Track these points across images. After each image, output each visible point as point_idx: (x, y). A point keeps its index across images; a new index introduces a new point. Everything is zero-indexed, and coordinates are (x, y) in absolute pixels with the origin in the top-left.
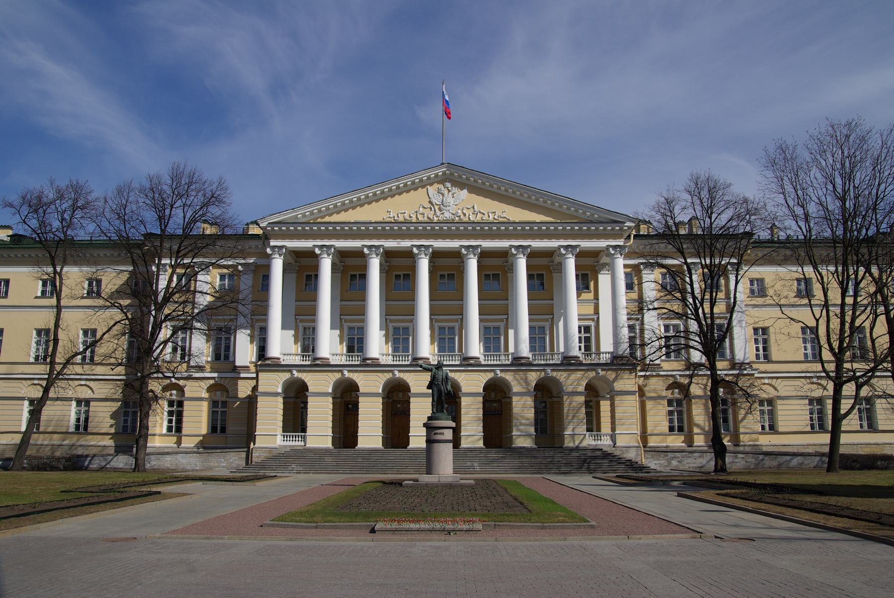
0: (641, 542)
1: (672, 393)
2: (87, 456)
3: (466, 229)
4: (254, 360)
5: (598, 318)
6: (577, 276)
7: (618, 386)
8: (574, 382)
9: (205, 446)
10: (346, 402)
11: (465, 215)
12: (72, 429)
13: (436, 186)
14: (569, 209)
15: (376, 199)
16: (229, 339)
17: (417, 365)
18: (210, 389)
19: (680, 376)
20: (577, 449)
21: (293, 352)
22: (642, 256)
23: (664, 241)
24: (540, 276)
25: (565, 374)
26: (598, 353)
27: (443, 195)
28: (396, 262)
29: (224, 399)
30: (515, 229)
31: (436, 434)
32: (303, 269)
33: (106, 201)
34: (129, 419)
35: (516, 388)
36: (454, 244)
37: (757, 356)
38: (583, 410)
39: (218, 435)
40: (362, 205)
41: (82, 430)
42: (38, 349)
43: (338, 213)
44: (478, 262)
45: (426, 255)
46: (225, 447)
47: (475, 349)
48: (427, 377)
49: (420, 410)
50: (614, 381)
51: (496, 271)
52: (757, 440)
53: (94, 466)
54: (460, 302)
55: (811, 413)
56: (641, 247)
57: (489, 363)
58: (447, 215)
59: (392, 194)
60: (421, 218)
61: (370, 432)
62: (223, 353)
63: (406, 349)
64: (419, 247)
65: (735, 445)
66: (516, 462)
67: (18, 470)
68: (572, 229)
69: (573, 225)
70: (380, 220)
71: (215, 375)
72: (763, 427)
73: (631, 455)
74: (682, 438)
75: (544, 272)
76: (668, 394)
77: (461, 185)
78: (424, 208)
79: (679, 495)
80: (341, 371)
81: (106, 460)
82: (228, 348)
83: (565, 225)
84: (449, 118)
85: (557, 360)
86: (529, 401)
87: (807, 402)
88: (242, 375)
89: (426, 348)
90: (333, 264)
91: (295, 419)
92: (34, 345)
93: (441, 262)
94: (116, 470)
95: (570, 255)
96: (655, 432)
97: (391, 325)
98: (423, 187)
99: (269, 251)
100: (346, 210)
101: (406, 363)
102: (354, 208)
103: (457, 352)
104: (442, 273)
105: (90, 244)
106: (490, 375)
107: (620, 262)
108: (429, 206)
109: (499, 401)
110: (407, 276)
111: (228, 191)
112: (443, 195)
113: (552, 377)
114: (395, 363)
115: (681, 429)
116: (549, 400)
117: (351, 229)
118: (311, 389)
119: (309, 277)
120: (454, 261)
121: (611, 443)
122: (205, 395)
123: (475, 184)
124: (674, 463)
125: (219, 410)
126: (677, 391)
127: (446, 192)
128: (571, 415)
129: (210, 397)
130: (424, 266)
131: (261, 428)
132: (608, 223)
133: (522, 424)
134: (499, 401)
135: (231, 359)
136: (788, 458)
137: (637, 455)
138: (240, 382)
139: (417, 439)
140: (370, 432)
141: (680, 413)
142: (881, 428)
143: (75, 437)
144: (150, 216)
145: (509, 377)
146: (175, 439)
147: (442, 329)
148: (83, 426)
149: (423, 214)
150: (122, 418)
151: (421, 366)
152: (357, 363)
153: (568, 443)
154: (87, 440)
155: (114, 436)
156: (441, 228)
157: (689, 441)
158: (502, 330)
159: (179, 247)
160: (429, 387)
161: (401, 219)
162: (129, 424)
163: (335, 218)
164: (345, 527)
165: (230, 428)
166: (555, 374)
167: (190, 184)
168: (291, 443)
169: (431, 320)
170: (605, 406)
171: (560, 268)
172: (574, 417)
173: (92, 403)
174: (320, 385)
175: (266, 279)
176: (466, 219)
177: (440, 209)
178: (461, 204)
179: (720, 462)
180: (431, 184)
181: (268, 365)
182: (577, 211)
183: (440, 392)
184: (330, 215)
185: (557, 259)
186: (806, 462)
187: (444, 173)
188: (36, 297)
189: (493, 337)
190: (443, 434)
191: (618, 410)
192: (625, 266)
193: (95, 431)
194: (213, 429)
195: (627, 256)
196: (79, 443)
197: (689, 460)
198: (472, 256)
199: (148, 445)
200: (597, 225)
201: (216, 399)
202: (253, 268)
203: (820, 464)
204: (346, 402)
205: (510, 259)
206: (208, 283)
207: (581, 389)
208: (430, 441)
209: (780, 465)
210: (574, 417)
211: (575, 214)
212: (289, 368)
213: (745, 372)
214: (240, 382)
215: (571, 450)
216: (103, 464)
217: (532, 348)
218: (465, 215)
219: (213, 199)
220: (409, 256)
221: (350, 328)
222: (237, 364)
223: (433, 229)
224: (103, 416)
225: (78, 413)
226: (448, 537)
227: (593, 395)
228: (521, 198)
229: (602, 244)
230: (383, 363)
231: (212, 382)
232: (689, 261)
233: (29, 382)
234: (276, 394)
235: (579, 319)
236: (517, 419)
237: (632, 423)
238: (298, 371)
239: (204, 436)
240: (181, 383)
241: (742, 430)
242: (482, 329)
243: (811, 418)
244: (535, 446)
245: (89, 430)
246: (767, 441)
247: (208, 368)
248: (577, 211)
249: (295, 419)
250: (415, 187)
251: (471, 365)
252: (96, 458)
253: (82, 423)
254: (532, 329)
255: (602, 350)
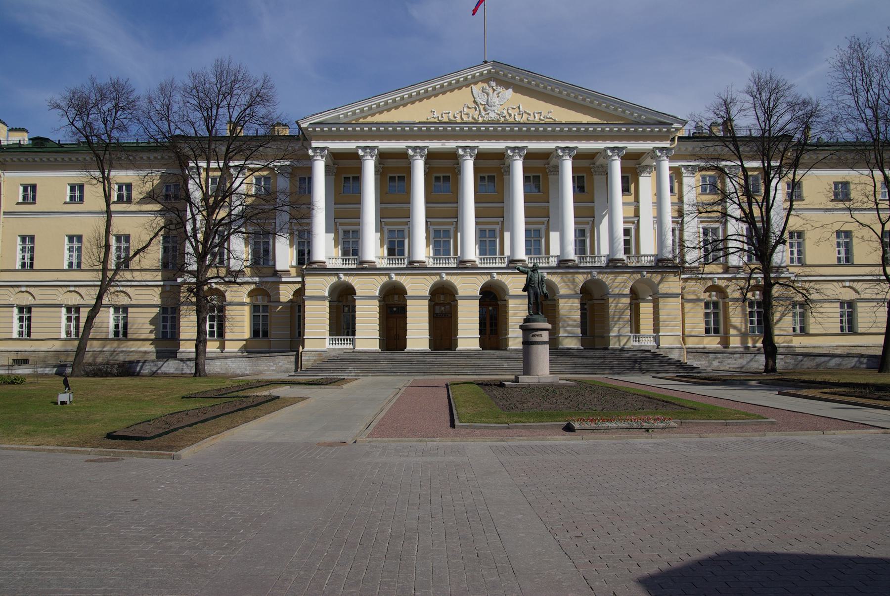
0: (767, 438)
1: (710, 296)
2: (138, 362)
3: (512, 130)
4: (294, 264)
5: (638, 221)
6: (573, 177)
7: (663, 288)
8: (619, 285)
9: (249, 350)
10: (393, 306)
11: (510, 115)
12: (111, 336)
13: (480, 85)
14: (616, 109)
15: (420, 98)
16: (268, 243)
17: (515, 268)
18: (250, 294)
19: (719, 279)
20: (622, 350)
21: (334, 256)
22: (700, 158)
23: (715, 143)
24: (537, 178)
25: (611, 276)
26: (638, 255)
27: (488, 95)
28: (390, 163)
29: (265, 303)
30: (562, 130)
31: (534, 336)
32: (345, 171)
33: (150, 102)
34: (169, 324)
35: (563, 291)
36: (400, 145)
37: (792, 260)
38: (628, 312)
39: (261, 340)
40: (405, 105)
41: (121, 336)
42: (71, 256)
43: (381, 112)
44: (474, 164)
45: (471, 156)
46: (272, 351)
47: (472, 252)
48: (522, 279)
49: (517, 311)
50: (660, 283)
51: (540, 173)
52: (791, 341)
53: (146, 371)
54: (454, 205)
55: (841, 316)
56: (690, 149)
57: (485, 266)
58: (493, 116)
59: (435, 93)
60: (465, 119)
61: (468, 334)
62: (263, 257)
63: (402, 252)
64: (464, 148)
65: (725, 348)
66: (570, 363)
67: (77, 376)
68: (619, 130)
69: (620, 126)
70: (424, 120)
71: (257, 279)
72: (794, 329)
73: (675, 355)
74: (718, 339)
75: (540, 174)
76: (705, 296)
77: (506, 85)
78: (468, 107)
79: (780, 394)
80: (388, 274)
81: (156, 365)
82: (266, 251)
83: (612, 126)
84: (473, 14)
85: (603, 262)
86: (576, 303)
87: (838, 305)
88: (284, 280)
89: (422, 251)
90: (327, 166)
91: (343, 322)
92: (66, 252)
93: (437, 163)
94: (166, 375)
95: (616, 158)
96: (693, 334)
97: (386, 228)
98: (467, 86)
99: (310, 152)
100: (389, 110)
101: (403, 266)
102: (397, 108)
103: (498, 255)
104: (438, 175)
105: (138, 148)
106: (487, 278)
107: (666, 165)
108: (473, 105)
109: (449, 304)
110: (401, 178)
111: (273, 90)
112: (488, 95)
113: (598, 279)
114: (391, 266)
115: (716, 331)
116: (590, 302)
117: (395, 130)
118: (358, 292)
119: (302, 180)
120: (448, 163)
121: (655, 344)
122: (246, 300)
123: (521, 84)
124: (715, 364)
125: (261, 314)
126: (714, 293)
127: (491, 91)
128: (616, 318)
129: (251, 302)
130: (370, 167)
131: (309, 331)
132: (657, 124)
133: (568, 325)
134: (449, 304)
135: (271, 263)
136: (826, 359)
137: (680, 356)
138: (282, 287)
139: (515, 339)
140: (468, 334)
141: (716, 315)
142: (812, 331)
143: (116, 343)
144: (197, 116)
145: (555, 279)
146: (217, 344)
147: (437, 232)
148: (122, 332)
149: (468, 114)
150: (162, 324)
151: (518, 269)
152: (453, 266)
153: (614, 344)
154: (127, 346)
155: (154, 342)
156: (487, 129)
157: (725, 342)
158: (543, 233)
159: (228, 149)
160: (524, 290)
161: (445, 119)
162: (168, 330)
163: (378, 118)
164: (537, 427)
165: (273, 332)
166: (601, 277)
167: (234, 82)
168: (340, 346)
169: (427, 222)
170: (646, 310)
171: (557, 170)
172: (619, 318)
173: (130, 310)
174: (368, 288)
175: (307, 181)
176: (511, 120)
177: (485, 110)
178: (507, 104)
179: (771, 363)
180: (476, 83)
181: (315, 269)
182: (624, 112)
183: (536, 295)
184: (373, 115)
185: (553, 161)
186: (844, 363)
187: (489, 71)
188: (66, 203)
189: (488, 241)
190: (541, 335)
191: (662, 312)
192: (671, 168)
193: (134, 337)
194: (255, 333)
195: (671, 159)
196: (120, 349)
197: (729, 361)
198: (518, 157)
199: (207, 350)
200: (645, 127)
201: (256, 303)
202: (290, 170)
203: (858, 365)
204: (393, 306)
205: (507, 161)
206: (245, 185)
207: (627, 291)
208: (527, 343)
209: (818, 365)
210: (619, 318)
211: (622, 115)
212: (335, 271)
213: (782, 275)
214: (282, 287)
215: (614, 351)
216: (154, 369)
217: (528, 252)
218: (510, 115)
219: (258, 98)
220: (453, 157)
221: (390, 231)
222: (278, 268)
223: (479, 129)
224: (142, 322)
225: (117, 319)
226: (646, 434)
227: (635, 297)
228: (568, 98)
229: (648, 146)
230: (378, 266)
231: (253, 287)
232: (747, 164)
233: (65, 289)
234: (322, 298)
235: (624, 222)
236: (565, 321)
237: (676, 325)
238: (345, 275)
239: (246, 340)
240: (222, 288)
241: (776, 332)
242: (432, 232)
243: (841, 320)
244: (581, 347)
245: (129, 336)
246: (800, 343)
247: (248, 271)
248: (624, 112)
249: (343, 322)
250: (459, 86)
251: (467, 268)
252: (147, 364)
253: (121, 329)
254: (527, 231)
255: (642, 253)
